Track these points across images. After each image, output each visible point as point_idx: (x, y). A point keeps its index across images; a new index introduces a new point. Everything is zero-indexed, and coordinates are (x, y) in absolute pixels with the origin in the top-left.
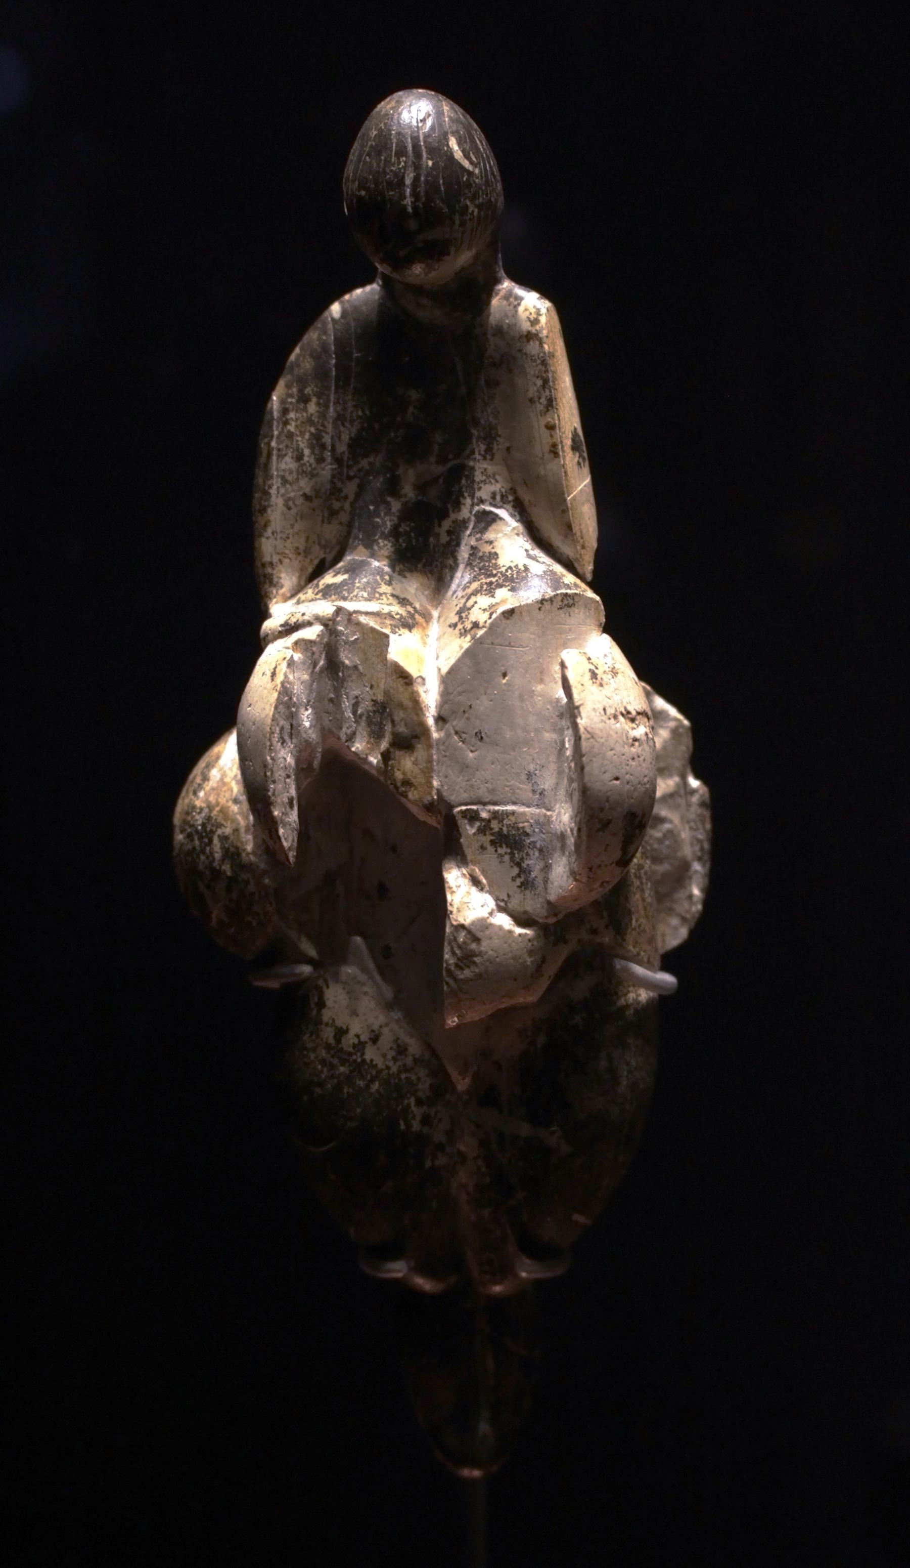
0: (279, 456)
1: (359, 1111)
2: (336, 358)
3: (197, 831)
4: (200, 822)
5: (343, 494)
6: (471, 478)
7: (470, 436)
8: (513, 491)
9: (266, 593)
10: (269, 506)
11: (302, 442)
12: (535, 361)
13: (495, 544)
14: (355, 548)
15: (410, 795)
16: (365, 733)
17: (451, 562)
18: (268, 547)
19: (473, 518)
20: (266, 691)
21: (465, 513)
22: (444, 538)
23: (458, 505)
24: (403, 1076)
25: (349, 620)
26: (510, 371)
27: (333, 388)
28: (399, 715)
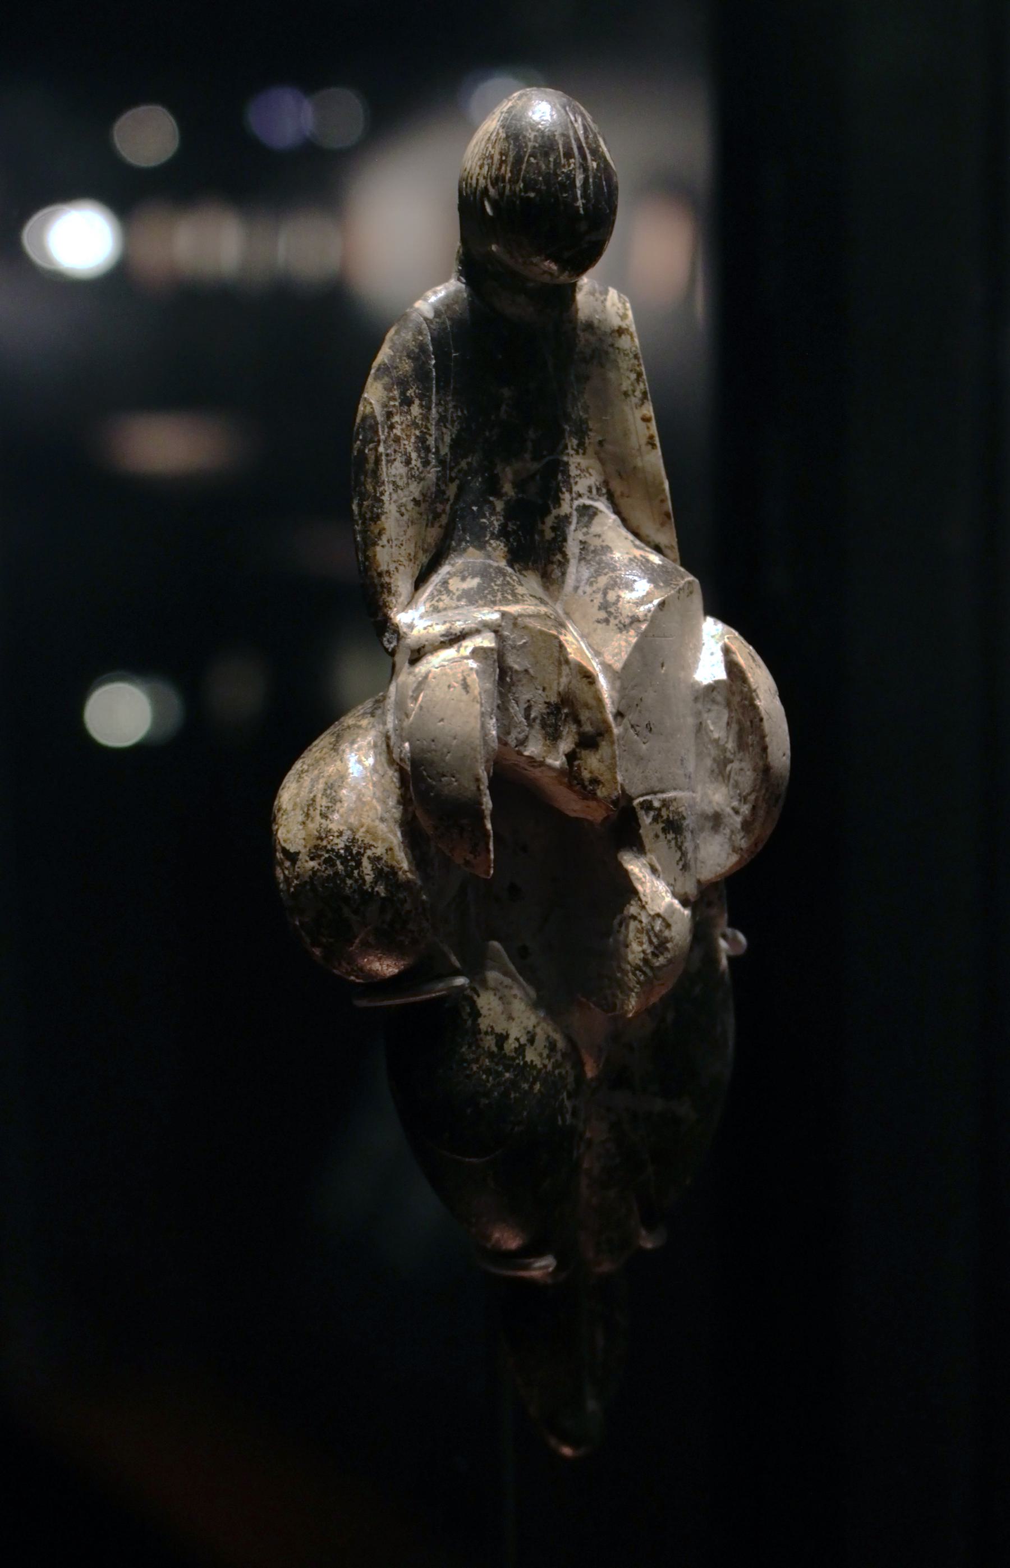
0: (388, 461)
1: (525, 1113)
2: (436, 359)
3: (338, 855)
4: (342, 845)
5: (446, 497)
6: (566, 473)
7: (562, 431)
8: (606, 483)
9: (385, 603)
10: (383, 513)
11: (409, 446)
12: (627, 355)
13: (604, 537)
14: (465, 550)
15: (599, 793)
16: (540, 737)
17: (559, 557)
18: (384, 555)
19: (575, 513)
20: (462, 704)
21: (565, 508)
22: (549, 535)
23: (558, 502)
24: (557, 1072)
25: (515, 625)
26: (602, 365)
27: (434, 390)
28: (584, 715)
